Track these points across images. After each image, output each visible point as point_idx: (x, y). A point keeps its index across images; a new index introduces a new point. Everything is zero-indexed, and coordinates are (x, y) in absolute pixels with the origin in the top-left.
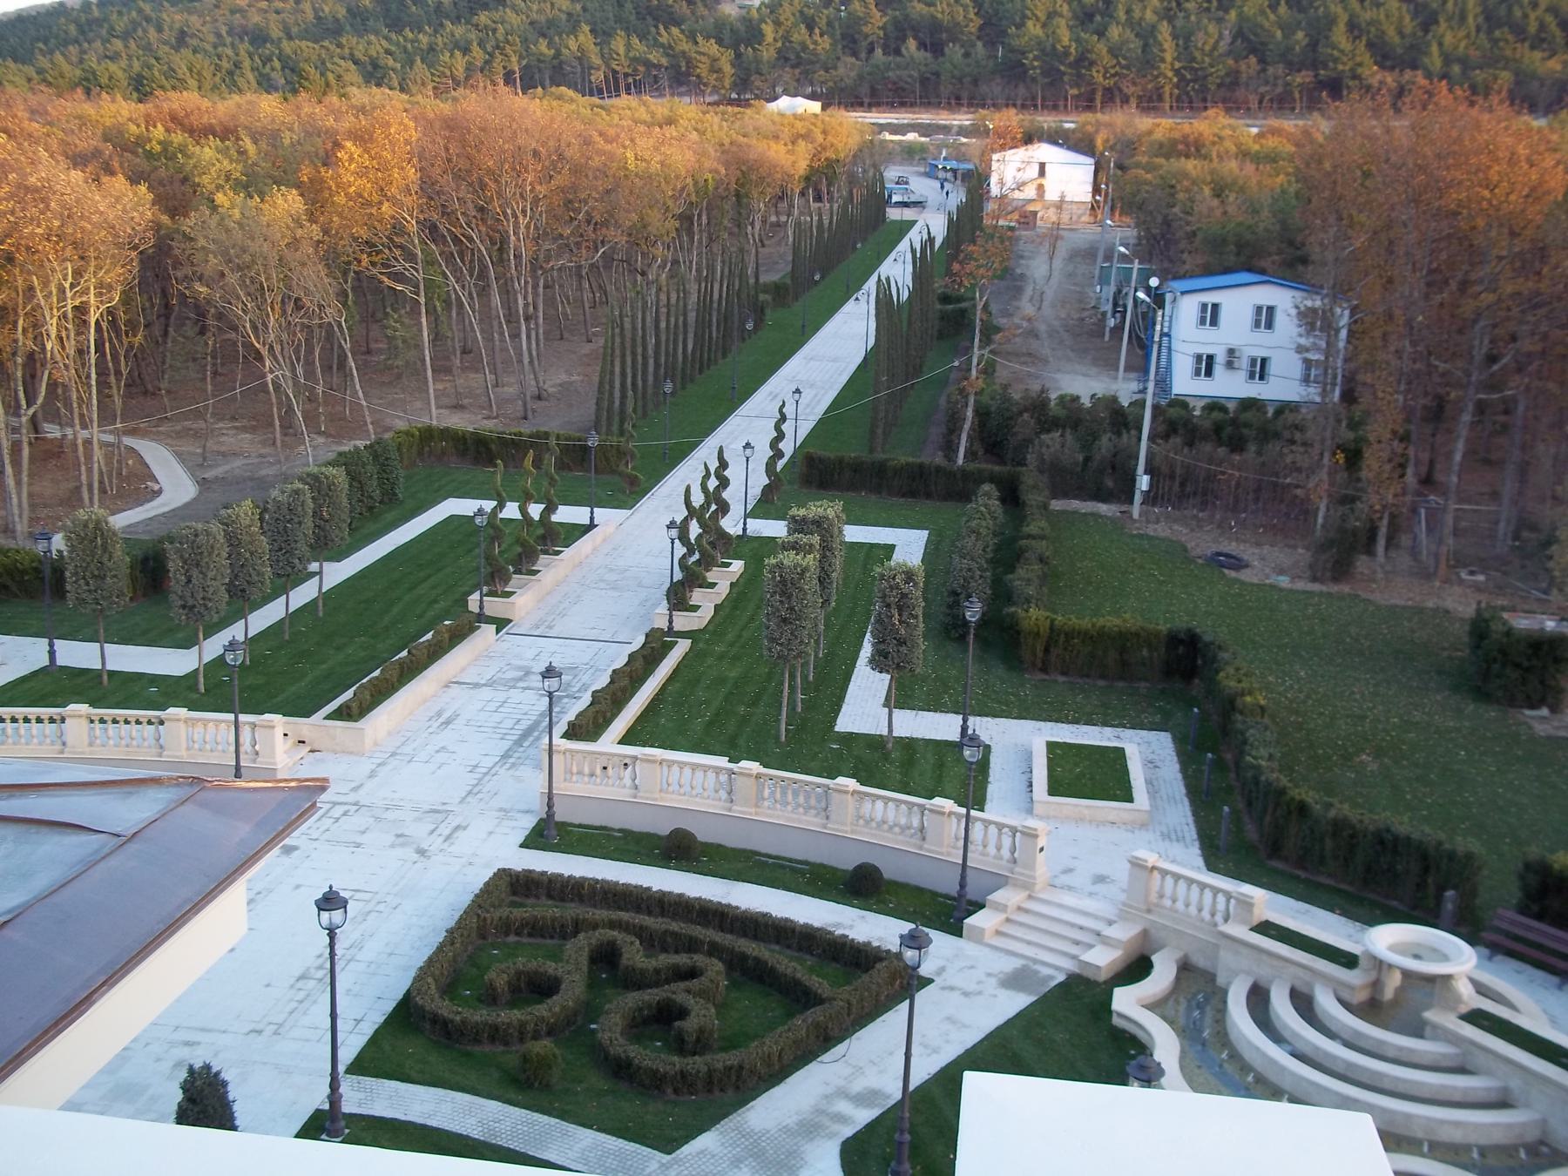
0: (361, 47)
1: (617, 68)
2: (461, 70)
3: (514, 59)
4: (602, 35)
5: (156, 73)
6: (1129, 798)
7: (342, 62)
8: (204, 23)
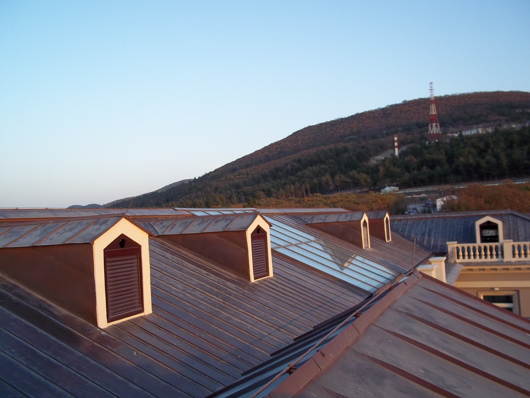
0: (265, 186)
1: (337, 184)
2: (293, 190)
3: (308, 185)
4: (333, 176)
5: (211, 201)
6: (255, 280)
7: (259, 192)
8: (222, 184)
